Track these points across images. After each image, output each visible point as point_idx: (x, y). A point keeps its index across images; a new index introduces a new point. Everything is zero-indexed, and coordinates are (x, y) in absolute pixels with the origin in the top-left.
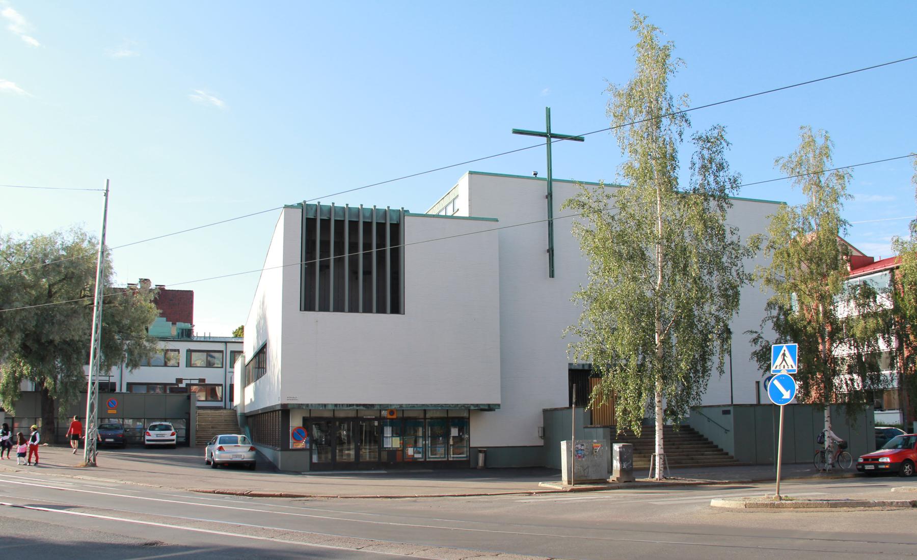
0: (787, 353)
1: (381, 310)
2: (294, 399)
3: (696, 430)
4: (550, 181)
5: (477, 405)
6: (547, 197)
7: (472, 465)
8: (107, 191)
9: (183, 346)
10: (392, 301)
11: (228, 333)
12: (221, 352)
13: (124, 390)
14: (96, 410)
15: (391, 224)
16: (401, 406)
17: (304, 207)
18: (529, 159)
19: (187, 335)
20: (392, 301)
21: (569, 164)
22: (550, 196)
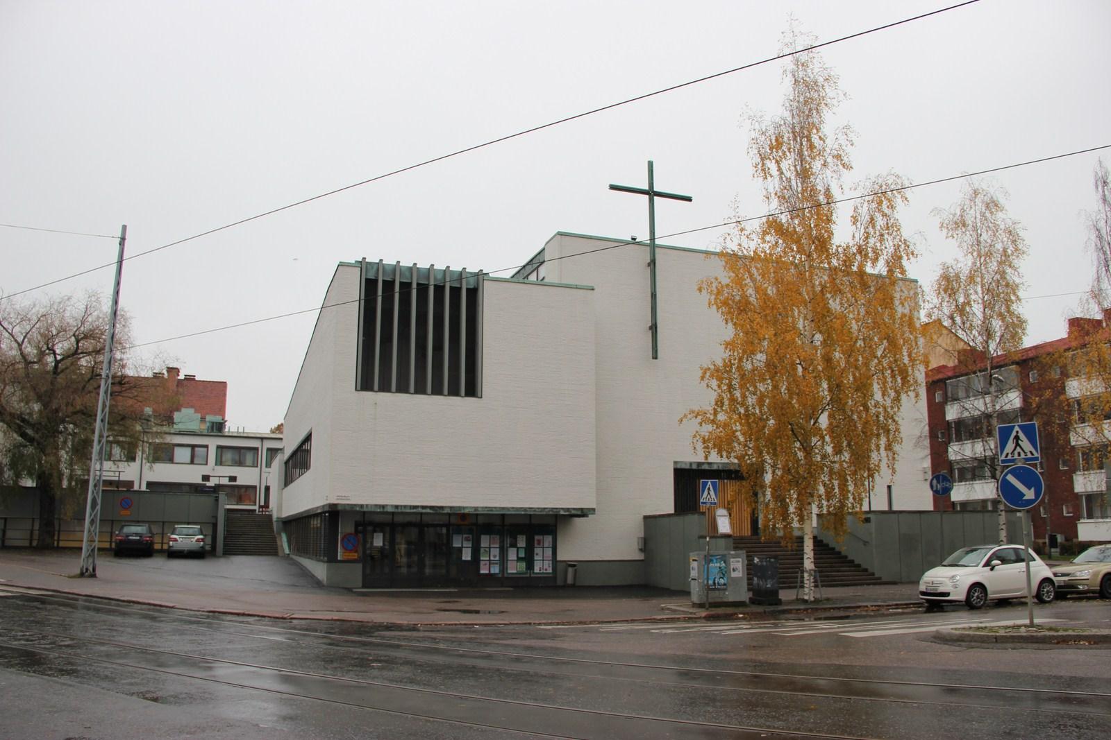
0: (1021, 435)
1: (454, 392)
2: (346, 498)
3: (825, 542)
4: (652, 245)
5: (568, 509)
6: (649, 265)
7: (560, 582)
8: (123, 239)
9: (213, 443)
10: (466, 382)
11: (265, 430)
12: (256, 449)
13: (144, 488)
14: (98, 507)
15: (468, 289)
16: (476, 509)
17: (363, 265)
18: (627, 218)
19: (218, 428)
20: (466, 382)
21: (675, 225)
22: (652, 264)
